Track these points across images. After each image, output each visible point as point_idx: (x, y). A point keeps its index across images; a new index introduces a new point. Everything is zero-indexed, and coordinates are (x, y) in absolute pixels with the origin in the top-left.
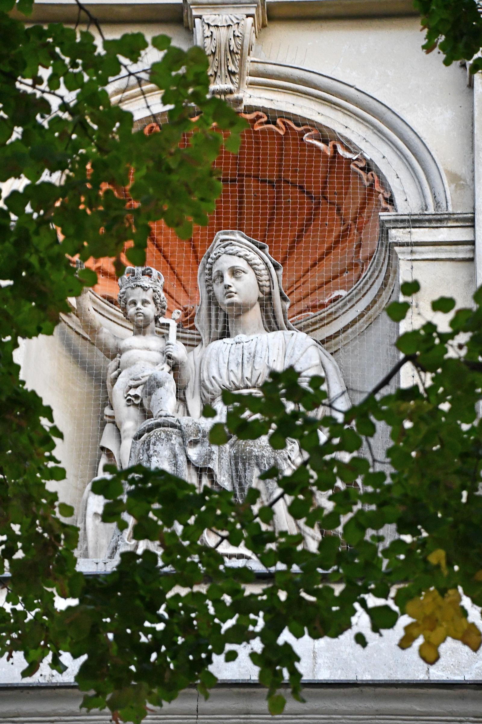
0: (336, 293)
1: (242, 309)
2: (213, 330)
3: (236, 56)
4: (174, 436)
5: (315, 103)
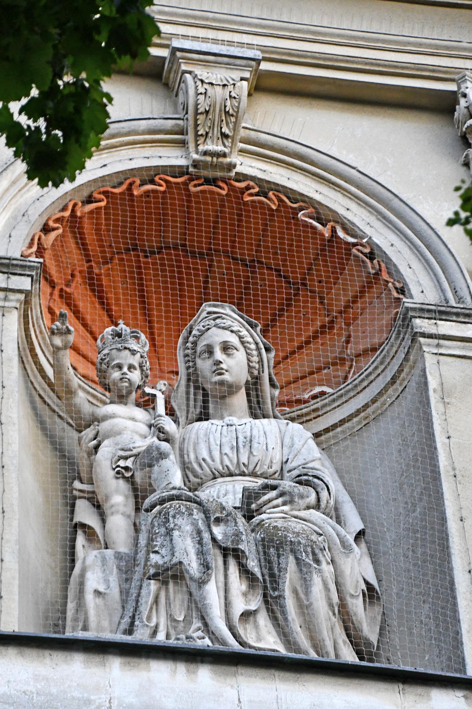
0: (317, 390)
1: (228, 390)
2: (191, 409)
3: (232, 118)
4: (195, 510)
5: (311, 180)
